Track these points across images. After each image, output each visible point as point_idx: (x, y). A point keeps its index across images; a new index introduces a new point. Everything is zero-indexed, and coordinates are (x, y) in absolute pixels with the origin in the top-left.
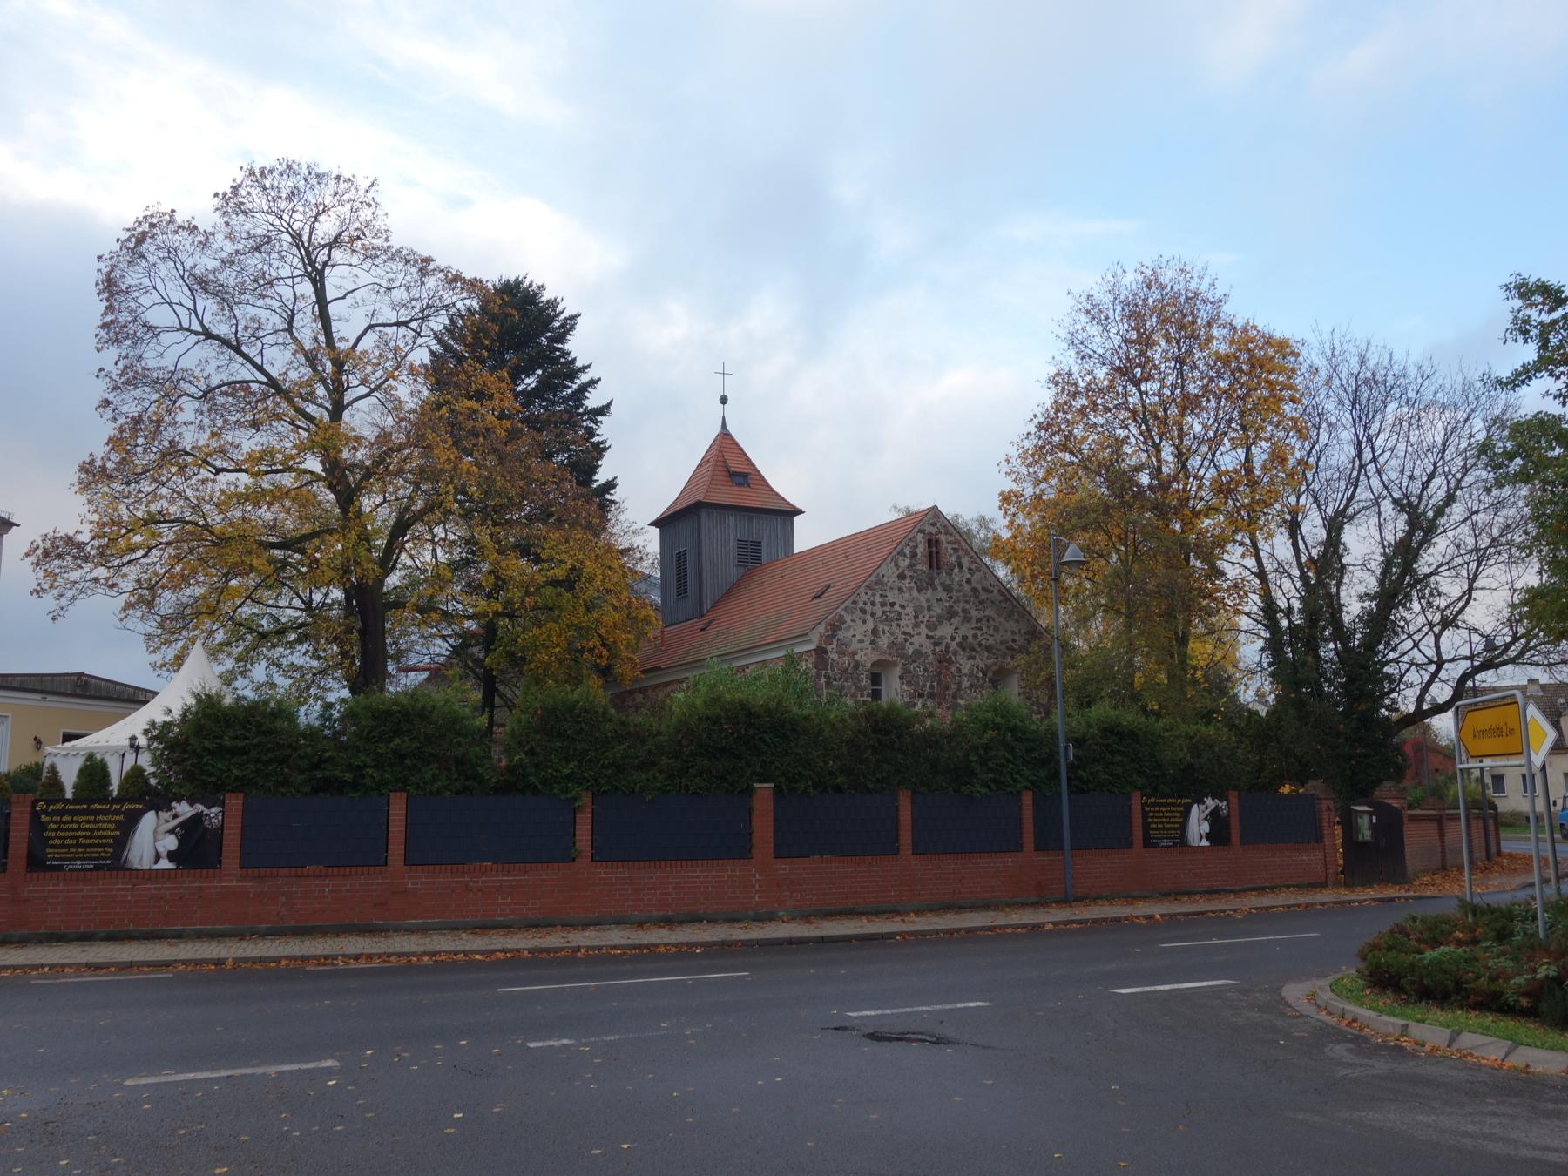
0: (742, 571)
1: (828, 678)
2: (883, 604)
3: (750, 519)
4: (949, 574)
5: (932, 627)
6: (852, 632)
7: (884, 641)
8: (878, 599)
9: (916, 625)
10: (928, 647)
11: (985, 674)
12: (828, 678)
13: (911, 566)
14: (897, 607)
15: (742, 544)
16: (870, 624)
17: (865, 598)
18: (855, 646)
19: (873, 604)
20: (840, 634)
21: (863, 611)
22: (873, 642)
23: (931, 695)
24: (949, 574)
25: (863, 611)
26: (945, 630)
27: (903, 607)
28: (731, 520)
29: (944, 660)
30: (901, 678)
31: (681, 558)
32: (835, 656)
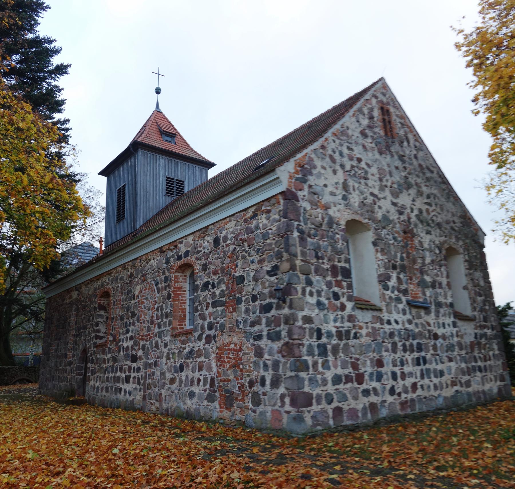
0: (169, 200)
1: (301, 232)
2: (351, 159)
3: (176, 164)
4: (401, 146)
5: (396, 195)
6: (321, 182)
7: (355, 199)
8: (346, 151)
9: (382, 188)
10: (394, 216)
11: (440, 250)
12: (301, 232)
13: (370, 127)
14: (363, 165)
15: (169, 181)
16: (340, 176)
17: (333, 145)
18: (327, 199)
19: (341, 154)
20: (312, 180)
21: (334, 161)
22: (345, 198)
23: (403, 269)
24: (401, 146)
25: (334, 161)
26: (405, 200)
27: (368, 165)
28: (161, 161)
29: (408, 233)
30: (375, 244)
31: (121, 193)
32: (306, 205)
